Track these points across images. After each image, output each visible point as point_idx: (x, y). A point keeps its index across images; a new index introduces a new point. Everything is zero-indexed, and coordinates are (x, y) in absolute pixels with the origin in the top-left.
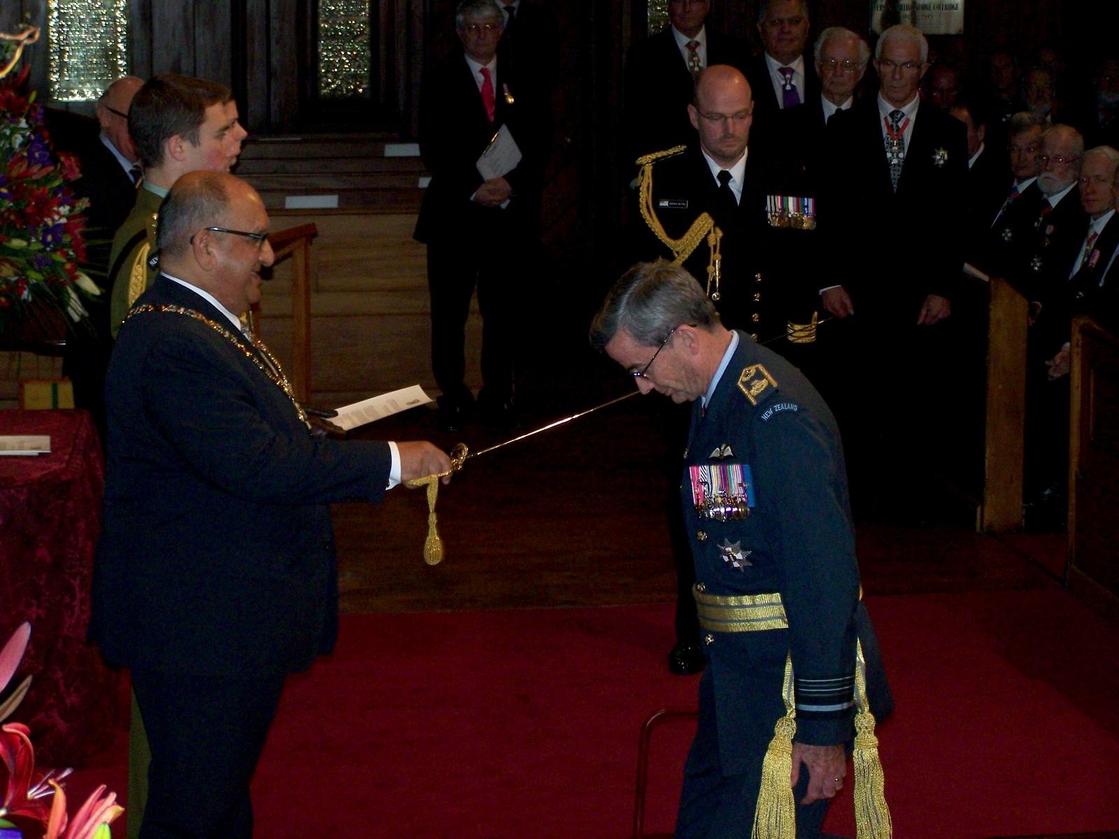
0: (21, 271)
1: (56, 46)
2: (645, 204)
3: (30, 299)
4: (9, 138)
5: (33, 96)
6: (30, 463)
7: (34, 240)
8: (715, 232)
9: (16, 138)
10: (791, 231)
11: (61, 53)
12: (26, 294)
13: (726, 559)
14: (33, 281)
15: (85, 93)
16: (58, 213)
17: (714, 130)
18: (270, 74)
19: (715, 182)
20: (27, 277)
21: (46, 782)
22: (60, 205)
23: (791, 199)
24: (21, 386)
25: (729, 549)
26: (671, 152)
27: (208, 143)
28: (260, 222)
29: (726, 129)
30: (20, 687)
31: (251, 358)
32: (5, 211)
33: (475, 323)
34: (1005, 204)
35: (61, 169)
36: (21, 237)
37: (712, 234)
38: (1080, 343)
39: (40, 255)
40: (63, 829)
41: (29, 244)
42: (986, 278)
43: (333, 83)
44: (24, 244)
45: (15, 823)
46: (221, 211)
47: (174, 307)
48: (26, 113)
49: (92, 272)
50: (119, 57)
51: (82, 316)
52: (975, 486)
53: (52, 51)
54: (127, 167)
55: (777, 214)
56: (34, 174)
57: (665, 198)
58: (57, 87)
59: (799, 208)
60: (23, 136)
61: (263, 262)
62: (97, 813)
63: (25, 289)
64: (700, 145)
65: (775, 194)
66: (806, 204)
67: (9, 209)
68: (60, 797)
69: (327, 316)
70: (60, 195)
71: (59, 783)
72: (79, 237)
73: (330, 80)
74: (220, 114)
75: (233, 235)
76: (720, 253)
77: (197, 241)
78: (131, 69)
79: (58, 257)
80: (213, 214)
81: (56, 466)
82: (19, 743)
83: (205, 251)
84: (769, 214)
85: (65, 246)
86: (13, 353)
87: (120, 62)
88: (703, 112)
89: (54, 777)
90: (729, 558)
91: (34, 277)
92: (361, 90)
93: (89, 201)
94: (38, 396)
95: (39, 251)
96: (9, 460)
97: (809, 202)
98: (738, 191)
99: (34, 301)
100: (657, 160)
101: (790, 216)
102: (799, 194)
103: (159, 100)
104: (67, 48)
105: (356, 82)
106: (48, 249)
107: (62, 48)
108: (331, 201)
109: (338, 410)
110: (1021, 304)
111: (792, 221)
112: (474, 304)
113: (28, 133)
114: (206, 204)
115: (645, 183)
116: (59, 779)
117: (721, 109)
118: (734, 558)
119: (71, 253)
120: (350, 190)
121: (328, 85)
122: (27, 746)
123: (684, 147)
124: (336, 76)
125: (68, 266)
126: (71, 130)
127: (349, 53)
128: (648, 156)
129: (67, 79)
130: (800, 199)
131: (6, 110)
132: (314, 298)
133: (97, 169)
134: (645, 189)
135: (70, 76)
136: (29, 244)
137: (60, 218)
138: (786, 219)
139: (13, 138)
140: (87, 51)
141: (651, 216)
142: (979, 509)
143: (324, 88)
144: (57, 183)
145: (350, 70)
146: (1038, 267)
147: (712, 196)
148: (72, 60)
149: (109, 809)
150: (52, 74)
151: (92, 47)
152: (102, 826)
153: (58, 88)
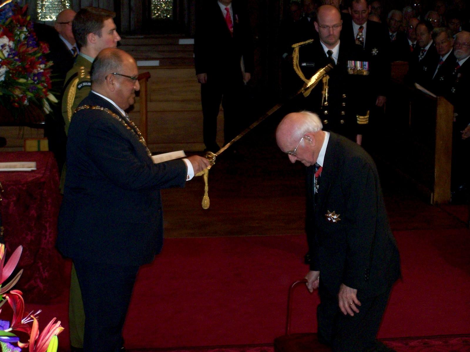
0: (24, 92)
3: (28, 104)
4: (19, 35)
5: (28, 18)
6: (27, 174)
7: (29, 79)
9: (22, 35)
10: (358, 76)
12: (26, 102)
13: (329, 219)
14: (29, 97)
15: (51, 18)
16: (40, 68)
17: (324, 32)
20: (26, 95)
21: (30, 316)
24: (25, 141)
25: (330, 215)
26: (307, 42)
27: (103, 39)
31: (130, 130)
32: (17, 67)
33: (221, 116)
39: (32, 86)
40: (37, 337)
43: (157, 13)
45: (16, 334)
51: (50, 112)
52: (431, 185)
54: (70, 47)
55: (353, 69)
57: (304, 62)
58: (40, 15)
60: (25, 34)
62: (52, 330)
63: (25, 100)
64: (319, 39)
65: (352, 60)
67: (19, 66)
69: (153, 112)
71: (35, 316)
72: (49, 78)
76: (328, 85)
77: (108, 79)
79: (40, 86)
81: (38, 176)
82: (18, 299)
85: (43, 81)
86: (21, 127)
87: (67, 4)
88: (320, 26)
89: (33, 314)
90: (331, 219)
91: (30, 95)
92: (168, 16)
93: (53, 63)
94: (32, 146)
95: (32, 84)
96: (13, 174)
97: (366, 63)
100: (301, 45)
102: (362, 60)
103: (84, 20)
106: (36, 83)
108: (156, 63)
112: (221, 107)
114: (113, 63)
115: (296, 55)
116: (35, 314)
118: (333, 218)
120: (164, 58)
121: (155, 14)
122: (21, 300)
123: (312, 40)
124: (158, 10)
125: (44, 90)
126: (45, 33)
128: (297, 44)
129: (44, 11)
132: (149, 104)
135: (45, 10)
139: (21, 35)
141: (298, 70)
142: (432, 194)
143: (154, 15)
144: (39, 55)
145: (164, 8)
148: (47, 3)
149: (58, 328)
150: (38, 9)
152: (54, 336)
153: (41, 15)
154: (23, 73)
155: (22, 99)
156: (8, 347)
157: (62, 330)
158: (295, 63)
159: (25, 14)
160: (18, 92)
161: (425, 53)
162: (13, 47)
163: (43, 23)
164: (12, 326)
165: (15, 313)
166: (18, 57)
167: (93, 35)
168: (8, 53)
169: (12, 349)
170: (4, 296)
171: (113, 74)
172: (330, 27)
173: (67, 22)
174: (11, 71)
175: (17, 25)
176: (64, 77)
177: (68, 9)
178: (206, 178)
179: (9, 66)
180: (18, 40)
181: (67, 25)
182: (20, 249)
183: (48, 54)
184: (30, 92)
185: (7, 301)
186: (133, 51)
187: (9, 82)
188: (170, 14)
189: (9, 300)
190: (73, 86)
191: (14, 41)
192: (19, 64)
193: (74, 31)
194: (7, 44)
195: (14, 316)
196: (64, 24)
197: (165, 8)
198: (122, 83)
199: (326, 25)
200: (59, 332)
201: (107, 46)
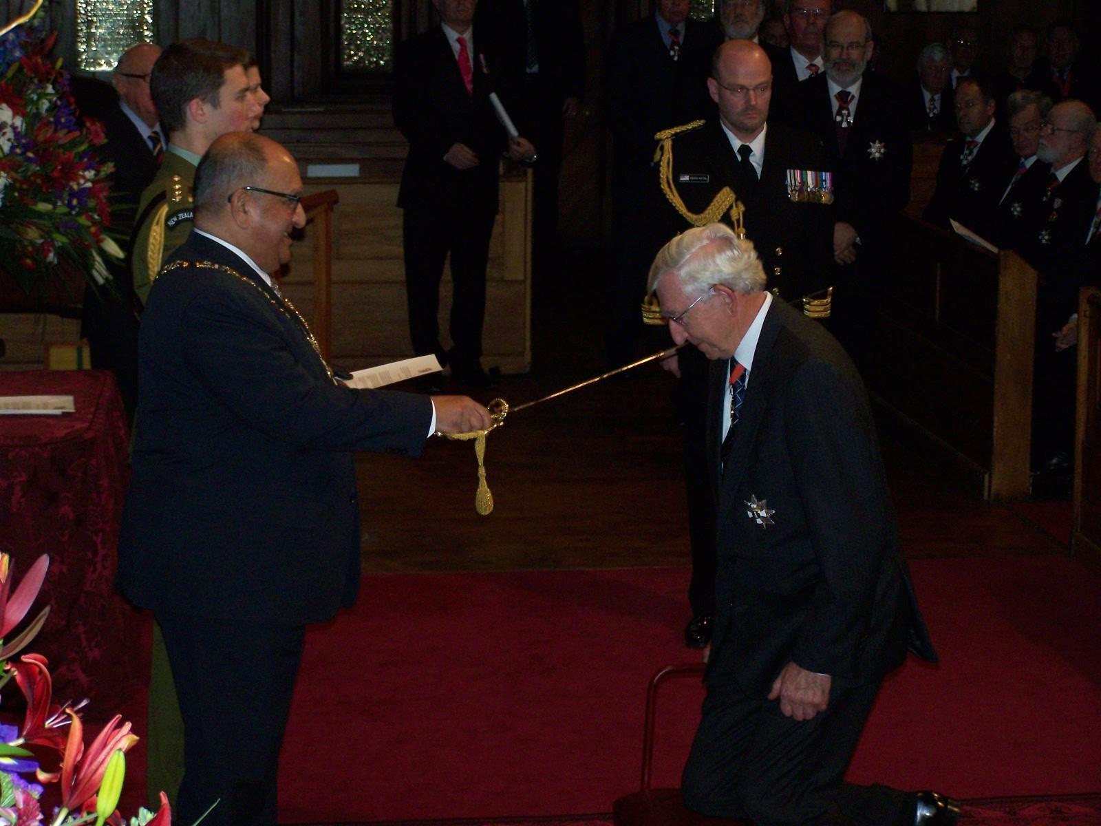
0: (47, 234)
1: (84, 17)
2: (665, 179)
3: (56, 261)
4: (36, 103)
5: (60, 63)
7: (59, 203)
8: (736, 206)
9: (43, 103)
11: (89, 24)
12: (51, 256)
14: (58, 244)
15: (105, 66)
16: (84, 177)
17: (736, 101)
18: (293, 44)
19: (736, 156)
20: (53, 240)
22: (86, 169)
23: (809, 173)
24: (47, 350)
28: (295, 185)
29: (748, 101)
30: (42, 613)
32: (32, 175)
34: (1014, 180)
35: (86, 134)
36: (46, 201)
37: (734, 208)
38: (1088, 313)
40: (79, 757)
41: (55, 207)
42: (994, 250)
43: (356, 55)
44: (50, 207)
46: (260, 171)
47: (209, 263)
48: (52, 78)
49: (118, 236)
50: (145, 28)
51: (106, 279)
53: (79, 21)
54: (145, 131)
56: (61, 138)
57: (685, 173)
58: (84, 57)
59: (818, 182)
60: (50, 101)
61: (296, 223)
63: (49, 251)
66: (824, 178)
67: (35, 174)
68: (76, 724)
70: (86, 160)
72: (104, 201)
73: (352, 52)
74: (238, 77)
75: (270, 195)
76: (744, 227)
77: (235, 199)
78: (157, 37)
79: (83, 220)
80: (251, 174)
83: (241, 209)
84: (789, 189)
85: (91, 210)
87: (147, 33)
89: (72, 706)
91: (60, 239)
94: (64, 358)
97: (827, 176)
98: (758, 165)
99: (59, 263)
100: (676, 134)
101: (809, 190)
102: (817, 169)
104: (95, 19)
105: (378, 55)
106: (74, 212)
107: (90, 19)
108: (352, 170)
109: (354, 373)
110: (1031, 274)
111: (811, 196)
113: (55, 99)
115: (665, 159)
116: (76, 709)
117: (742, 80)
119: (96, 217)
121: (351, 56)
122: (45, 676)
123: (702, 122)
124: (358, 48)
125: (93, 230)
126: (93, 97)
127: (372, 26)
129: (94, 49)
130: (818, 173)
131: (33, 75)
133: (110, 137)
134: (666, 164)
135: (97, 46)
136: (55, 207)
137: (85, 182)
138: (806, 193)
139: (40, 103)
140: (114, 22)
142: (987, 477)
143: (348, 60)
144: (83, 148)
145: (373, 42)
146: (1046, 240)
147: (732, 170)
148: (100, 31)
149: (125, 738)
151: (119, 19)
152: (117, 752)
154: (44, 190)
155: (42, 250)
156: (14, 783)
157: (134, 741)
158: (663, 175)
159: (51, 56)
160: (33, 234)
161: (975, 151)
162: (22, 128)
163: (91, 76)
164: (25, 733)
165: (30, 705)
166: (33, 153)
167: (200, 103)
168: (10, 144)
169: (25, 787)
170: (8, 667)
171: (245, 188)
172: (748, 90)
173: (142, 74)
174: (18, 185)
175: (31, 78)
176: (137, 201)
177: (148, 44)
178: (480, 449)
179: (13, 174)
180: (34, 114)
181: (141, 80)
182: (44, 563)
183: (103, 146)
184: (60, 233)
185: (13, 678)
186: (298, 141)
187: (15, 210)
188: (385, 59)
189: (18, 678)
190: (157, 224)
191: (24, 115)
192: (40, 165)
193: (155, 97)
194: (9, 122)
195: (28, 712)
196: (135, 79)
197: (375, 42)
198: (265, 211)
199: (738, 85)
200: (127, 745)
201: (231, 129)
